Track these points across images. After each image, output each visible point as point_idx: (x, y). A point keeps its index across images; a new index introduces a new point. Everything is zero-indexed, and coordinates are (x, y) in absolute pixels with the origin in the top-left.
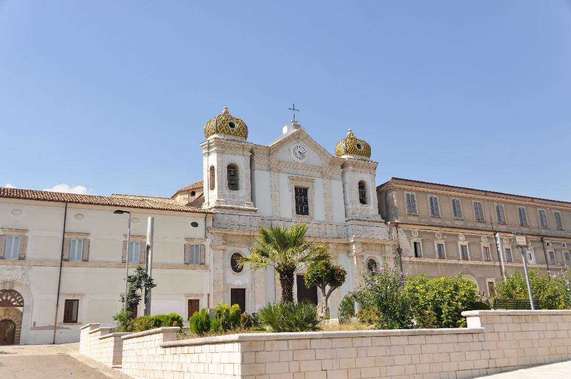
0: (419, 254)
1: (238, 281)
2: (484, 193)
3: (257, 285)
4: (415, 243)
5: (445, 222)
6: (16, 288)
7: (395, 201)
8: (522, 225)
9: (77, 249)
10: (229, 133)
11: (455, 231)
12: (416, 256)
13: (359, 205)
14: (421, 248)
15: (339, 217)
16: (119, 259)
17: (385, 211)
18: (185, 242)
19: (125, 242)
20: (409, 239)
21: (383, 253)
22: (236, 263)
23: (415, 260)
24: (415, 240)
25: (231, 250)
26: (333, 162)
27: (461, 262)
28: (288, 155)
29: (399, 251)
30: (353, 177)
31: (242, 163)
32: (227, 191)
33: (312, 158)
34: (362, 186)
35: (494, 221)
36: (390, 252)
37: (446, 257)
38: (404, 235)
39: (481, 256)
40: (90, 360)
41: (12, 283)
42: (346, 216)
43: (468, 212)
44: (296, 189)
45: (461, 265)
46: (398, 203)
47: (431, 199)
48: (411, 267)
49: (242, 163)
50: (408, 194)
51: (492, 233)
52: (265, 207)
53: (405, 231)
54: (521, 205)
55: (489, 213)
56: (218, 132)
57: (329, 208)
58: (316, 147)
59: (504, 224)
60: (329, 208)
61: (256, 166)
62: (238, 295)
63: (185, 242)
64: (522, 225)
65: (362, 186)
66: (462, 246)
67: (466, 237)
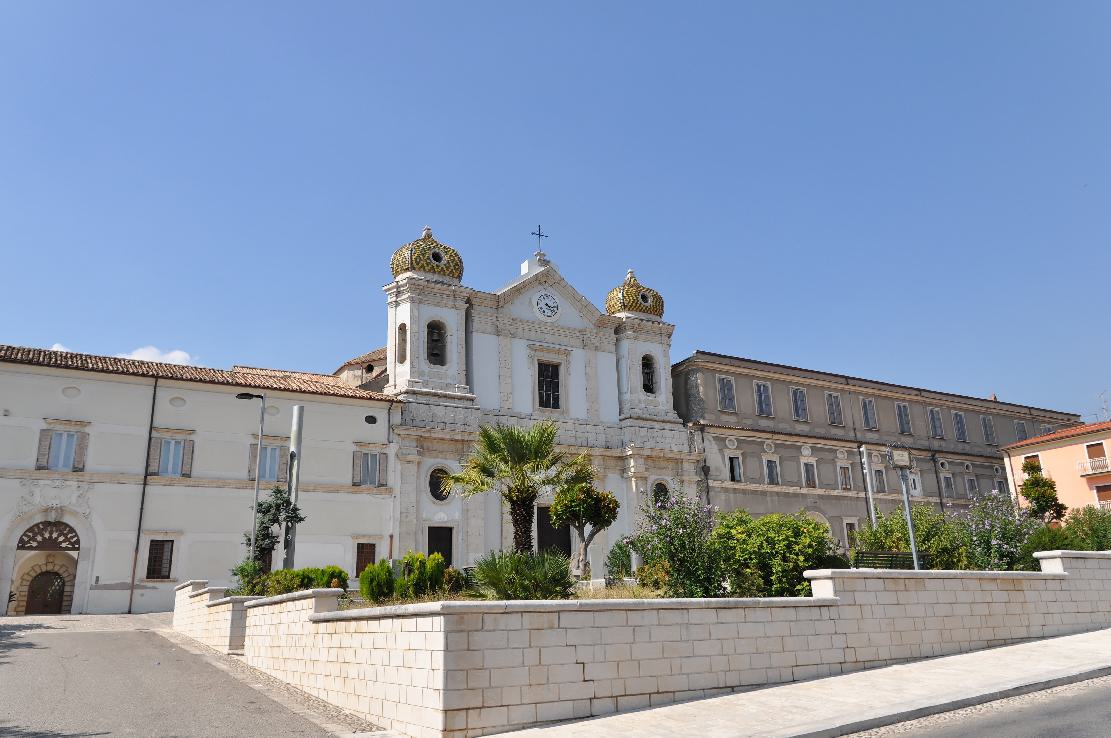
0: (737, 478)
4: (731, 459)
5: (817, 430)
7: (701, 389)
9: (172, 458)
10: (433, 270)
13: (642, 395)
15: (610, 414)
16: (30, 462)
18: (355, 448)
22: (437, 485)
25: (431, 463)
28: (528, 309)
30: (634, 349)
31: (453, 321)
34: (648, 363)
35: (858, 426)
41: (61, 510)
43: (818, 410)
44: (541, 365)
45: (804, 496)
46: (705, 394)
48: (723, 496)
49: (453, 321)
51: (855, 445)
52: (488, 395)
57: (592, 398)
60: (592, 398)
61: (476, 324)
62: (440, 538)
63: (355, 448)
65: (648, 363)
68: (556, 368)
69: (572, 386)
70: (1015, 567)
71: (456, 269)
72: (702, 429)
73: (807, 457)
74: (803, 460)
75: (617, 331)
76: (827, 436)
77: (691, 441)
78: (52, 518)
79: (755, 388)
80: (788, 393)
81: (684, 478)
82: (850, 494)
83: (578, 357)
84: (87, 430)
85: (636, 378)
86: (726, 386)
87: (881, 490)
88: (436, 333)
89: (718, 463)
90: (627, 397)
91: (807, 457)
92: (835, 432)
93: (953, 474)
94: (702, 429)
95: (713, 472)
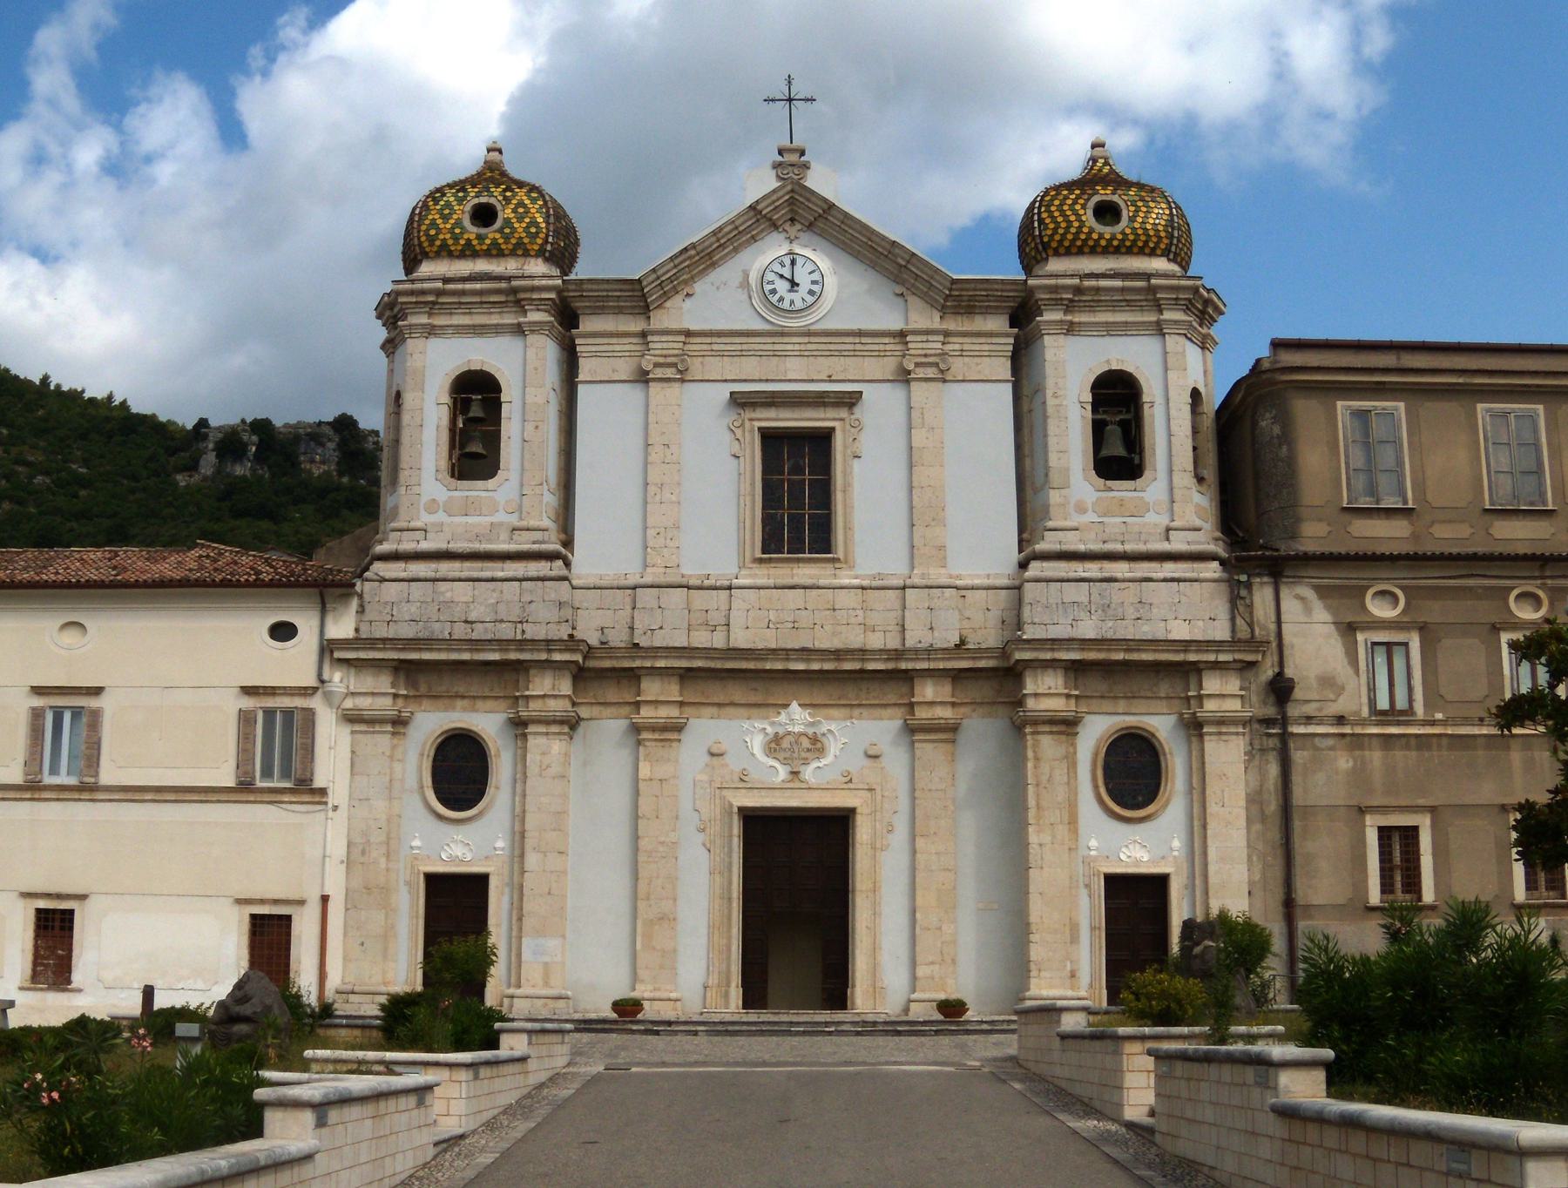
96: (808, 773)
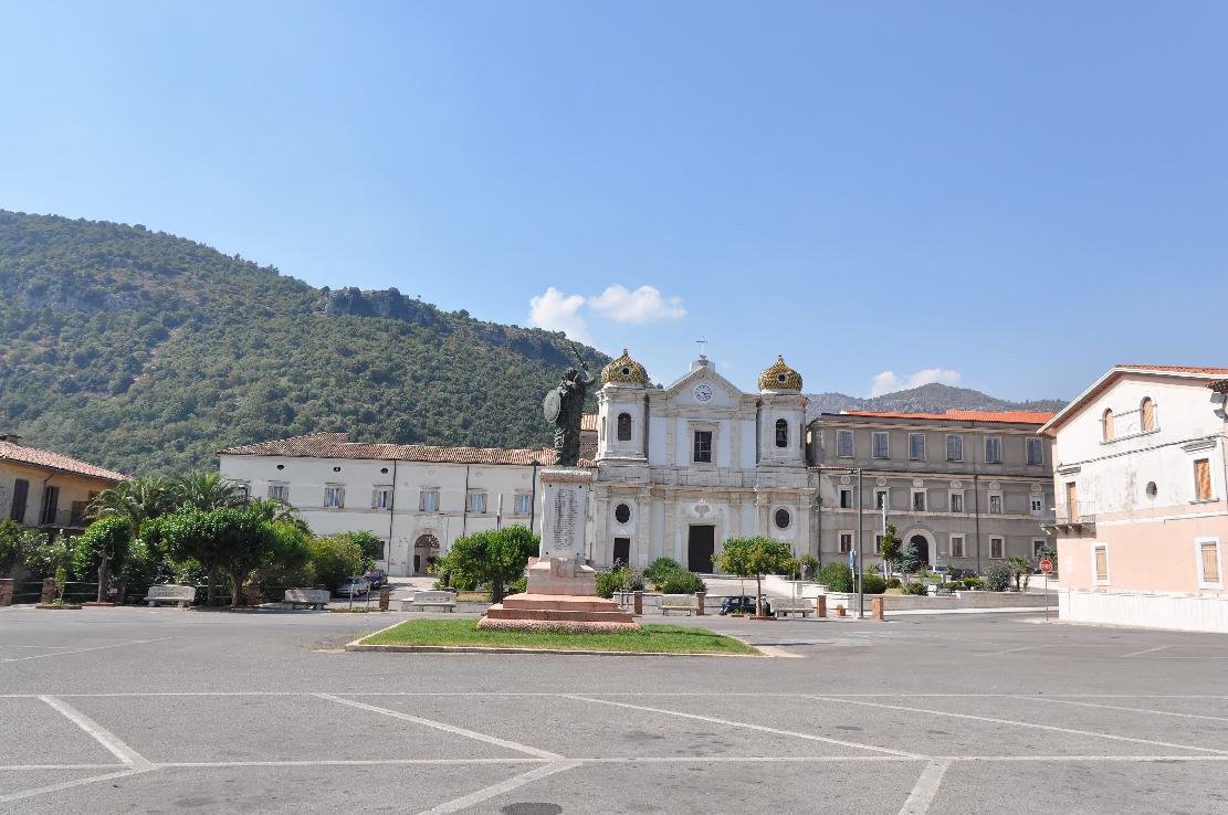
0: (847, 504)
1: (623, 531)
2: (969, 424)
3: (641, 536)
4: (843, 493)
5: (896, 464)
6: (434, 534)
7: (823, 442)
8: (1031, 463)
9: (477, 505)
10: (623, 381)
11: (909, 476)
12: (843, 505)
13: (775, 449)
14: (851, 497)
15: (748, 461)
16: (417, 506)
17: (810, 456)
18: (374, 488)
19: (374, 492)
20: (835, 486)
21: (797, 502)
22: (623, 514)
23: (841, 510)
24: (845, 488)
25: (616, 501)
26: (745, 398)
27: (913, 513)
28: (689, 397)
29: (819, 500)
30: (770, 417)
31: (636, 412)
32: (616, 442)
33: (719, 397)
34: (782, 425)
35: (978, 459)
36: (806, 503)
37: (926, 508)
38: (830, 483)
39: (946, 505)
40: (1102, 625)
41: (430, 530)
42: (757, 461)
43: (936, 450)
44: (697, 433)
45: (911, 517)
46: (826, 444)
47: (989, 442)
48: (833, 518)
49: (636, 412)
50: (878, 435)
51: (973, 477)
52: (658, 455)
53: (831, 477)
54: (881, 430)
55: (899, 449)
56: (610, 380)
57: (736, 453)
58: (726, 385)
59: (997, 463)
60: (736, 453)
61: (652, 410)
62: (622, 547)
63: (374, 488)
64: (1031, 463)
65: (782, 425)
66: (916, 495)
67: (926, 482)
68: (709, 435)
69: (721, 449)
70: (154, 592)
71: (797, 381)
72: (819, 472)
73: (918, 486)
74: (913, 491)
75: (758, 405)
76: (964, 471)
77: (810, 478)
78: (428, 533)
79: (985, 442)
80: (906, 440)
81: (801, 506)
82: (959, 515)
83: (726, 425)
84: (439, 491)
85: (769, 435)
86: (880, 440)
87: (892, 507)
88: (624, 421)
89: (831, 493)
90: (763, 450)
91: (918, 486)
92: (952, 466)
93: (1004, 493)
94: (819, 472)
95: (825, 501)
96: (705, 515)
